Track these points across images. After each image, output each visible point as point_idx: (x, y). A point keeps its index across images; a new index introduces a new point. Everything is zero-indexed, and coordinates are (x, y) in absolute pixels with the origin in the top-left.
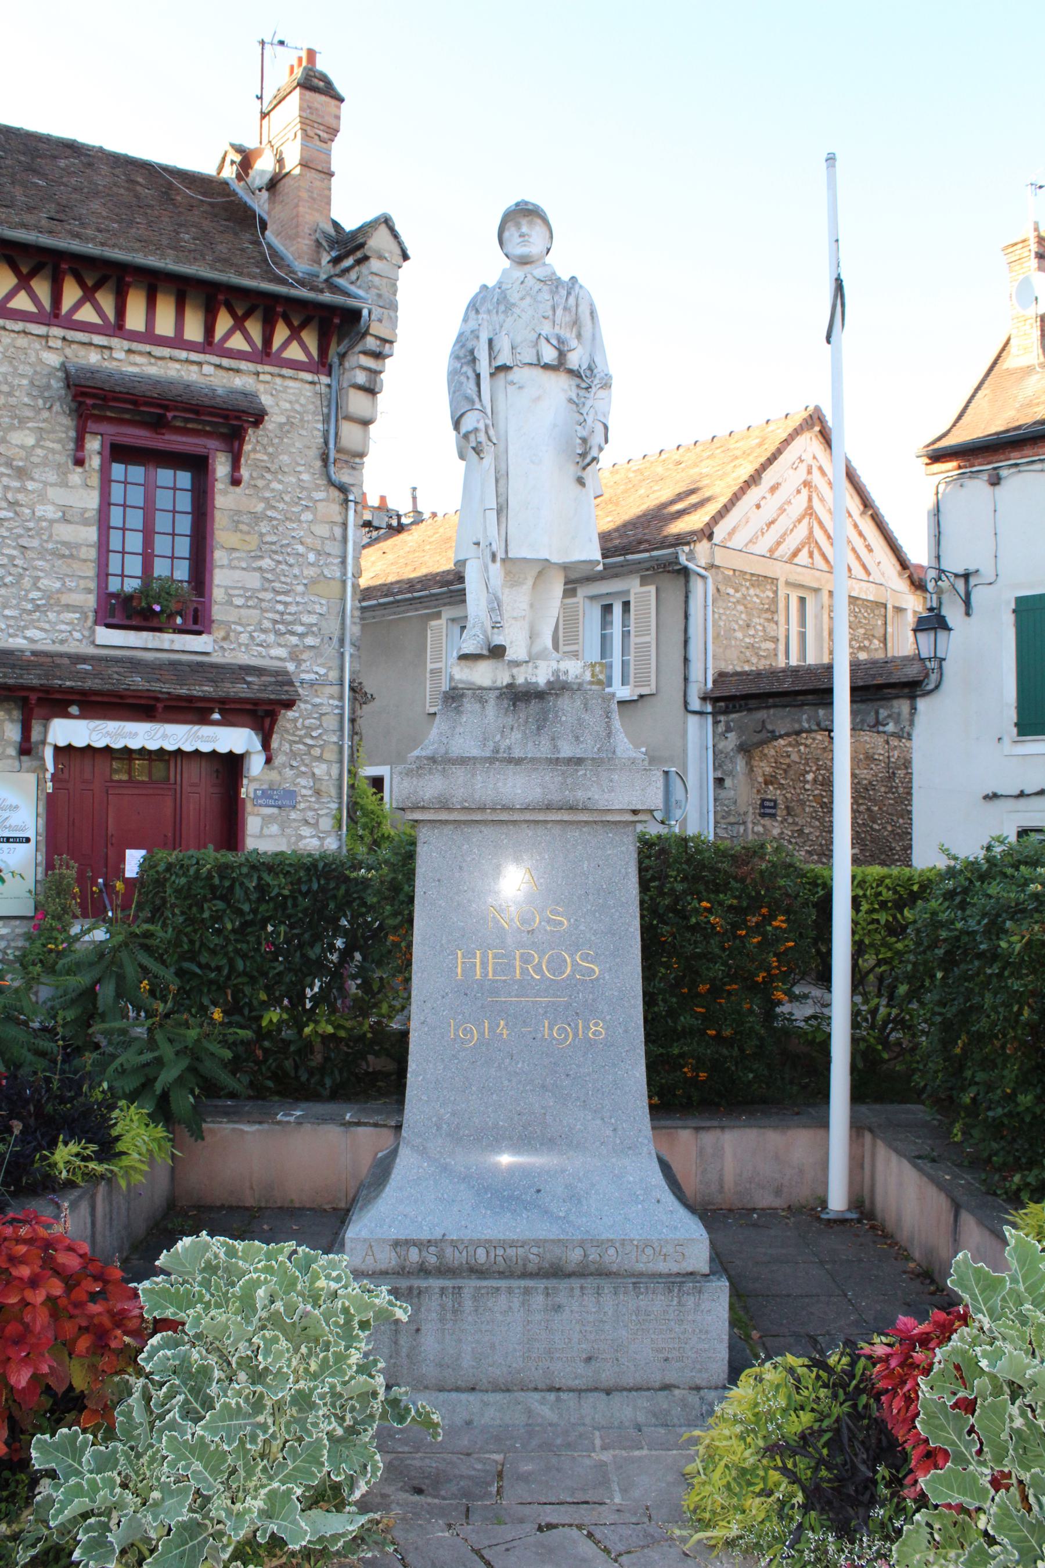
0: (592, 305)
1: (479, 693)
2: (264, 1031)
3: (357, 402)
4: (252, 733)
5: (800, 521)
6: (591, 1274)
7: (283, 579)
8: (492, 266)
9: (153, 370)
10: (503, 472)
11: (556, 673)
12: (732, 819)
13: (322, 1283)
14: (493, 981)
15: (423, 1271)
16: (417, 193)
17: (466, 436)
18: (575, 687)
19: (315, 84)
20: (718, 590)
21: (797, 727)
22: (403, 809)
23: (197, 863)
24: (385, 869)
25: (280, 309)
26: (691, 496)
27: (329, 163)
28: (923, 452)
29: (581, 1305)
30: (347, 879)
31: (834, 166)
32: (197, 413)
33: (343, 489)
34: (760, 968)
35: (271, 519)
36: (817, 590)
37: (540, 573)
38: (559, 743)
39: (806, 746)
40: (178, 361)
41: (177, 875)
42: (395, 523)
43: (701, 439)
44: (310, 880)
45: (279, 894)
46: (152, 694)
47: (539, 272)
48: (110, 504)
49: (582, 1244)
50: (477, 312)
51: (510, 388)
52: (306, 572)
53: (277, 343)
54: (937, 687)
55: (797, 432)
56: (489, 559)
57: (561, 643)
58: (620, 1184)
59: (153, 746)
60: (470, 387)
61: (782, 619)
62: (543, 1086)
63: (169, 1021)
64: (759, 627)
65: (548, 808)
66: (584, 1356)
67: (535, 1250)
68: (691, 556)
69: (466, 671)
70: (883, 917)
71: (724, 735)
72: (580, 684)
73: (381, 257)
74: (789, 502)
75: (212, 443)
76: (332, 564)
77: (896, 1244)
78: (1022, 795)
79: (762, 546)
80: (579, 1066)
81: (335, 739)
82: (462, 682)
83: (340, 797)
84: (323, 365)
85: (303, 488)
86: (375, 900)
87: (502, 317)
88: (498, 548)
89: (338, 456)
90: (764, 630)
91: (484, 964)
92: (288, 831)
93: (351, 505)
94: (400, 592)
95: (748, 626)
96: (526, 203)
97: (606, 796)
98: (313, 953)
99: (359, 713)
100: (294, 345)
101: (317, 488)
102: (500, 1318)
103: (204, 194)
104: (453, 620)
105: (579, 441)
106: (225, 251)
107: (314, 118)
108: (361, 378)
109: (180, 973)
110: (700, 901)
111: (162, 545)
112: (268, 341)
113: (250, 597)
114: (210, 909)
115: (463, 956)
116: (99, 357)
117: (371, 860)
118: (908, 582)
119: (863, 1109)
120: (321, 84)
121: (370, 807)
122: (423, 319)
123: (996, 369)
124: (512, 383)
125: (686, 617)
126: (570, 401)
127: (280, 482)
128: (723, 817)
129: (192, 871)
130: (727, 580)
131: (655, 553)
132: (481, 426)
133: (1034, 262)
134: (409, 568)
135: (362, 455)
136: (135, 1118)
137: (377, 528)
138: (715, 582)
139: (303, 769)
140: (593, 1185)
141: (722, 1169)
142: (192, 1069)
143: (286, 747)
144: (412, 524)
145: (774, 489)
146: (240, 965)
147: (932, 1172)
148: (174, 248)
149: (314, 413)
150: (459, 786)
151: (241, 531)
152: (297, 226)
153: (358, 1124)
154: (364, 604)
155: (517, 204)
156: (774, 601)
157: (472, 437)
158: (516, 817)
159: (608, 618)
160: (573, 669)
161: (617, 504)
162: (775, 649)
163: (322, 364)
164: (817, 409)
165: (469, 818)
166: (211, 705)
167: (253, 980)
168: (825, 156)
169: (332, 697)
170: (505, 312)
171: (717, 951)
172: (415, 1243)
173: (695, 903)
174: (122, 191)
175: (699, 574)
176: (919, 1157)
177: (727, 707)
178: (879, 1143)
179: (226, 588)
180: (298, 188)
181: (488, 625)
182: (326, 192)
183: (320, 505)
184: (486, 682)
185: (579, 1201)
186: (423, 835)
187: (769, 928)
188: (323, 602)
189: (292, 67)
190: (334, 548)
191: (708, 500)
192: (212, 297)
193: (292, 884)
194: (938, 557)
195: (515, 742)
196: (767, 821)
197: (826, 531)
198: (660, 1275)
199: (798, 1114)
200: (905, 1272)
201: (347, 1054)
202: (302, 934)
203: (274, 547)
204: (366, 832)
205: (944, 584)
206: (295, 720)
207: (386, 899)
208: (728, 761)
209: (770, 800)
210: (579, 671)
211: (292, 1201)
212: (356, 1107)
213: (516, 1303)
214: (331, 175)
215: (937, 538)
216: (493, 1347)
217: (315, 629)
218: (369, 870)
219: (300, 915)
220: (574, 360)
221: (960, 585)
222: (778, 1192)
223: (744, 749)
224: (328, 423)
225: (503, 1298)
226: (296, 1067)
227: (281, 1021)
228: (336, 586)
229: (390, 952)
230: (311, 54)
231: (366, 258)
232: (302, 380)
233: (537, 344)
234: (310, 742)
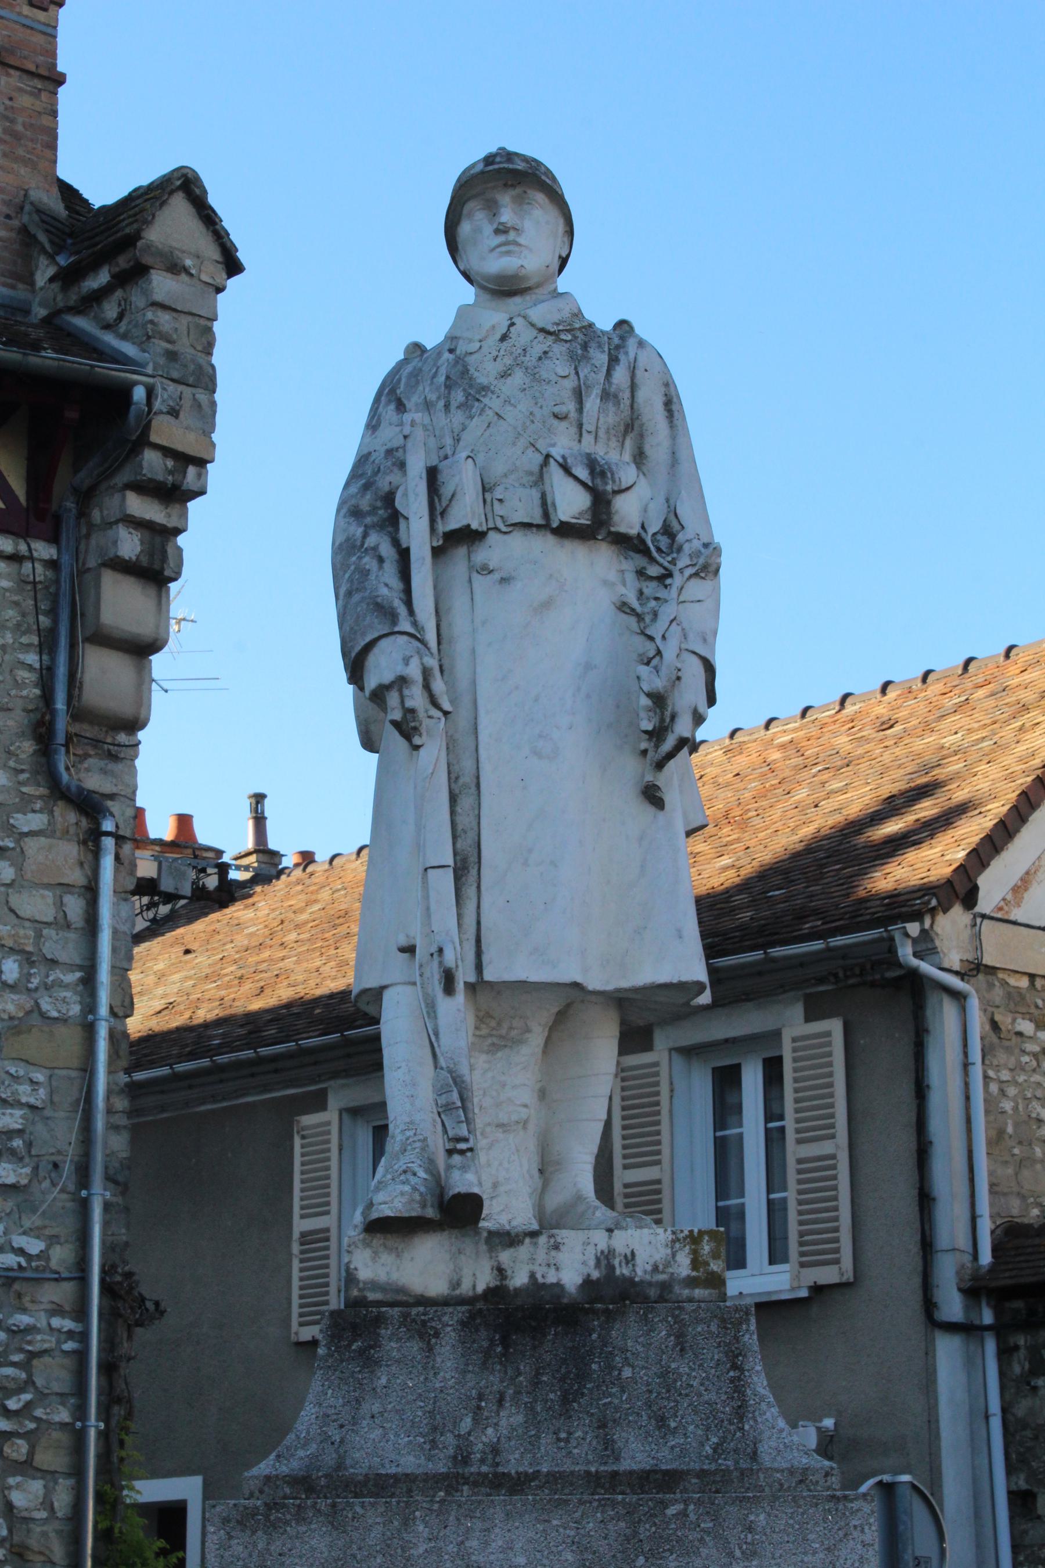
1: (418, 1314)
3: (120, 603)
8: (434, 302)
10: (467, 778)
17: (378, 696)
18: (653, 1293)
20: (995, 1026)
26: (919, 802)
27: (53, 55)
37: (561, 1017)
38: (618, 1435)
42: (212, 882)
43: (938, 665)
47: (543, 313)
50: (401, 407)
56: (437, 988)
57: (618, 1162)
60: (385, 583)
68: (926, 946)
69: (386, 1258)
72: (665, 1287)
73: (175, 268)
76: (60, 984)
81: (63, 1415)
82: (374, 1285)
87: (458, 417)
88: (459, 958)
89: (75, 728)
93: (109, 843)
94: (227, 1046)
96: (509, 156)
99: (125, 1348)
101: (25, 804)
105: (645, 701)
108: (129, 545)
124: (486, 570)
126: (623, 607)
130: (1016, 1001)
131: (838, 941)
132: (414, 671)
134: (248, 987)
135: (135, 724)
137: (170, 898)
138: (987, 1006)
144: (255, 880)
149: (19, 629)
154: (140, 1076)
155: (489, 160)
157: (393, 699)
159: (731, 1099)
160: (646, 1247)
161: (743, 824)
169: (57, 1311)
181: (438, 1145)
182: (45, 120)
183: (31, 846)
184: (436, 1287)
188: (39, 1077)
190: (64, 947)
195: (506, 1432)
210: (661, 1254)
214: (60, 80)
217: (17, 1143)
220: (630, 512)
228: (70, 1039)
231: (139, 271)
233: (539, 476)
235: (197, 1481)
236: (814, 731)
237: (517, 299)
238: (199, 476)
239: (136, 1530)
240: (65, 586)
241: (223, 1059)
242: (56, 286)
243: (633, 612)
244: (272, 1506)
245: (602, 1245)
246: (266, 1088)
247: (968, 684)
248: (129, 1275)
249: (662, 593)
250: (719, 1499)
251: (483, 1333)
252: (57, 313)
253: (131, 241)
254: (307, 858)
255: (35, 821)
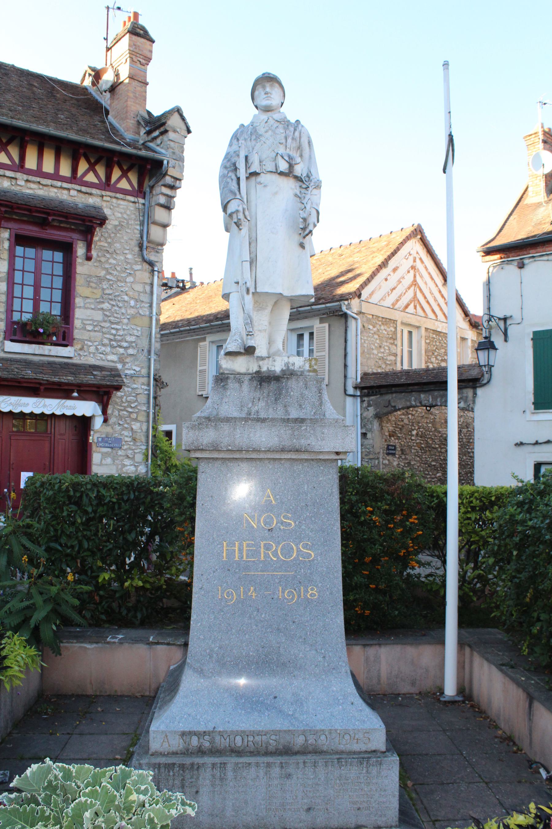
0: (309, 137)
1: (238, 377)
2: (100, 585)
3: (160, 214)
4: (96, 404)
5: (409, 288)
6: (310, 753)
7: (115, 315)
8: (247, 114)
9: (41, 192)
10: (254, 238)
11: (287, 364)
12: (371, 456)
13: (134, 797)
14: (246, 562)
15: (201, 752)
16: (198, 94)
17: (231, 215)
18: (299, 374)
19: (138, 32)
20: (364, 326)
21: (408, 404)
22: (189, 451)
23: (60, 482)
24: (175, 487)
25: (116, 159)
27: (146, 77)
28: (481, 249)
29: (304, 774)
30: (152, 492)
31: (448, 69)
32: (66, 217)
33: (151, 264)
34: (401, 548)
35: (109, 280)
36: (418, 327)
37: (276, 303)
39: (412, 415)
40: (55, 187)
41: (47, 490)
44: (129, 493)
45: (110, 501)
46: (37, 381)
47: (276, 116)
48: (14, 270)
49: (304, 733)
50: (238, 140)
51: (258, 186)
52: (129, 312)
53: (114, 178)
54: (488, 382)
55: (408, 238)
58: (328, 695)
59: (37, 411)
60: (233, 185)
61: (399, 344)
62: (278, 629)
63: (40, 581)
64: (387, 348)
65: (283, 450)
66: (305, 807)
67: (273, 737)
68: (349, 307)
69: (230, 362)
70: (473, 516)
71: (366, 409)
73: (175, 131)
74: (403, 278)
75: (75, 236)
77: (488, 717)
78: (537, 443)
79: (388, 302)
80: (301, 616)
81: (145, 408)
82: (227, 369)
83: (147, 442)
84: (141, 192)
85: (128, 263)
86: (169, 505)
87: (253, 143)
88: (251, 285)
89: (148, 245)
90: (389, 349)
91: (240, 550)
92: (117, 462)
93: (156, 273)
94: (183, 326)
95: (380, 347)
96: (269, 74)
97: (319, 443)
98: (131, 537)
99: (159, 393)
100: (124, 180)
101: (136, 263)
102: (251, 783)
103: (73, 94)
104: (213, 342)
106: (84, 125)
107: (137, 51)
109: (48, 550)
110: (366, 506)
111: (45, 294)
112: (108, 177)
113: (96, 326)
114: (67, 510)
115: (227, 545)
116: (9, 184)
117: (166, 480)
118: (468, 324)
119: (463, 632)
120: (142, 32)
121: (165, 448)
122: (199, 166)
123: (520, 204)
124: (260, 183)
125: (346, 341)
126: (296, 195)
127: (115, 259)
128: (366, 455)
129: (56, 487)
130: (369, 321)
131: (328, 305)
132: (241, 209)
133: (541, 145)
134: (188, 313)
135: (162, 245)
136: (17, 643)
137: (171, 288)
139: (126, 426)
140: (310, 693)
141: (379, 670)
142: (54, 611)
143: (116, 413)
145: (395, 270)
146: (86, 545)
147: (512, 674)
148: (54, 123)
150: (226, 436)
151: (91, 287)
152: (127, 112)
153: (158, 643)
154: (162, 332)
155: (264, 74)
156: (395, 333)
157: (235, 216)
158: (262, 456)
159: (301, 343)
162: (395, 360)
163: (140, 192)
164: (419, 226)
165: (231, 456)
166: (70, 388)
167: (93, 554)
168: (442, 63)
169: (143, 384)
170: (255, 140)
171: (377, 537)
172: (195, 733)
173: (363, 508)
174: (25, 90)
175: (353, 317)
176: (503, 665)
177: (369, 393)
178: (475, 654)
179: (82, 320)
180: (128, 91)
181: (244, 333)
182: (144, 94)
183: (138, 273)
184: (243, 370)
185: (302, 704)
186: (202, 467)
187: (408, 523)
188: (139, 329)
189: (125, 23)
191: (359, 275)
192: (75, 151)
193: (118, 495)
194: (489, 309)
196: (390, 458)
197: (423, 294)
198: (354, 753)
199: (424, 635)
200: (496, 737)
201: (151, 598)
202: (124, 526)
203: (110, 297)
204: (162, 463)
205: (493, 323)
206: (122, 397)
207: (175, 504)
208: (369, 423)
209: (392, 446)
210: (302, 363)
211: (116, 691)
212: (157, 632)
213: (262, 773)
214: (147, 84)
215: (488, 297)
216: (246, 802)
217: (134, 344)
218: (165, 486)
219: (123, 514)
220: (299, 170)
221: (502, 324)
222: (413, 684)
223: (378, 416)
224: (143, 216)
225: (253, 770)
226: (120, 607)
227: (111, 579)
228: (147, 320)
229: (177, 536)
230: (136, 15)
231: (166, 131)
232: (128, 201)
233: (274, 162)
234: (130, 410)
235: (175, 425)
236: (323, 256)
237: (270, 113)
238: (180, 183)
239: (161, 436)
240: (146, 210)
241: (182, 329)
242: (146, 135)
243: (299, 197)
244: (200, 424)
245: (286, 361)
246: (192, 336)
247: (360, 246)
248: (160, 376)
249: (306, 192)
250: (315, 426)
251: (255, 382)
252: (146, 142)
253: (164, 124)
254: (202, 283)
255: (139, 267)
